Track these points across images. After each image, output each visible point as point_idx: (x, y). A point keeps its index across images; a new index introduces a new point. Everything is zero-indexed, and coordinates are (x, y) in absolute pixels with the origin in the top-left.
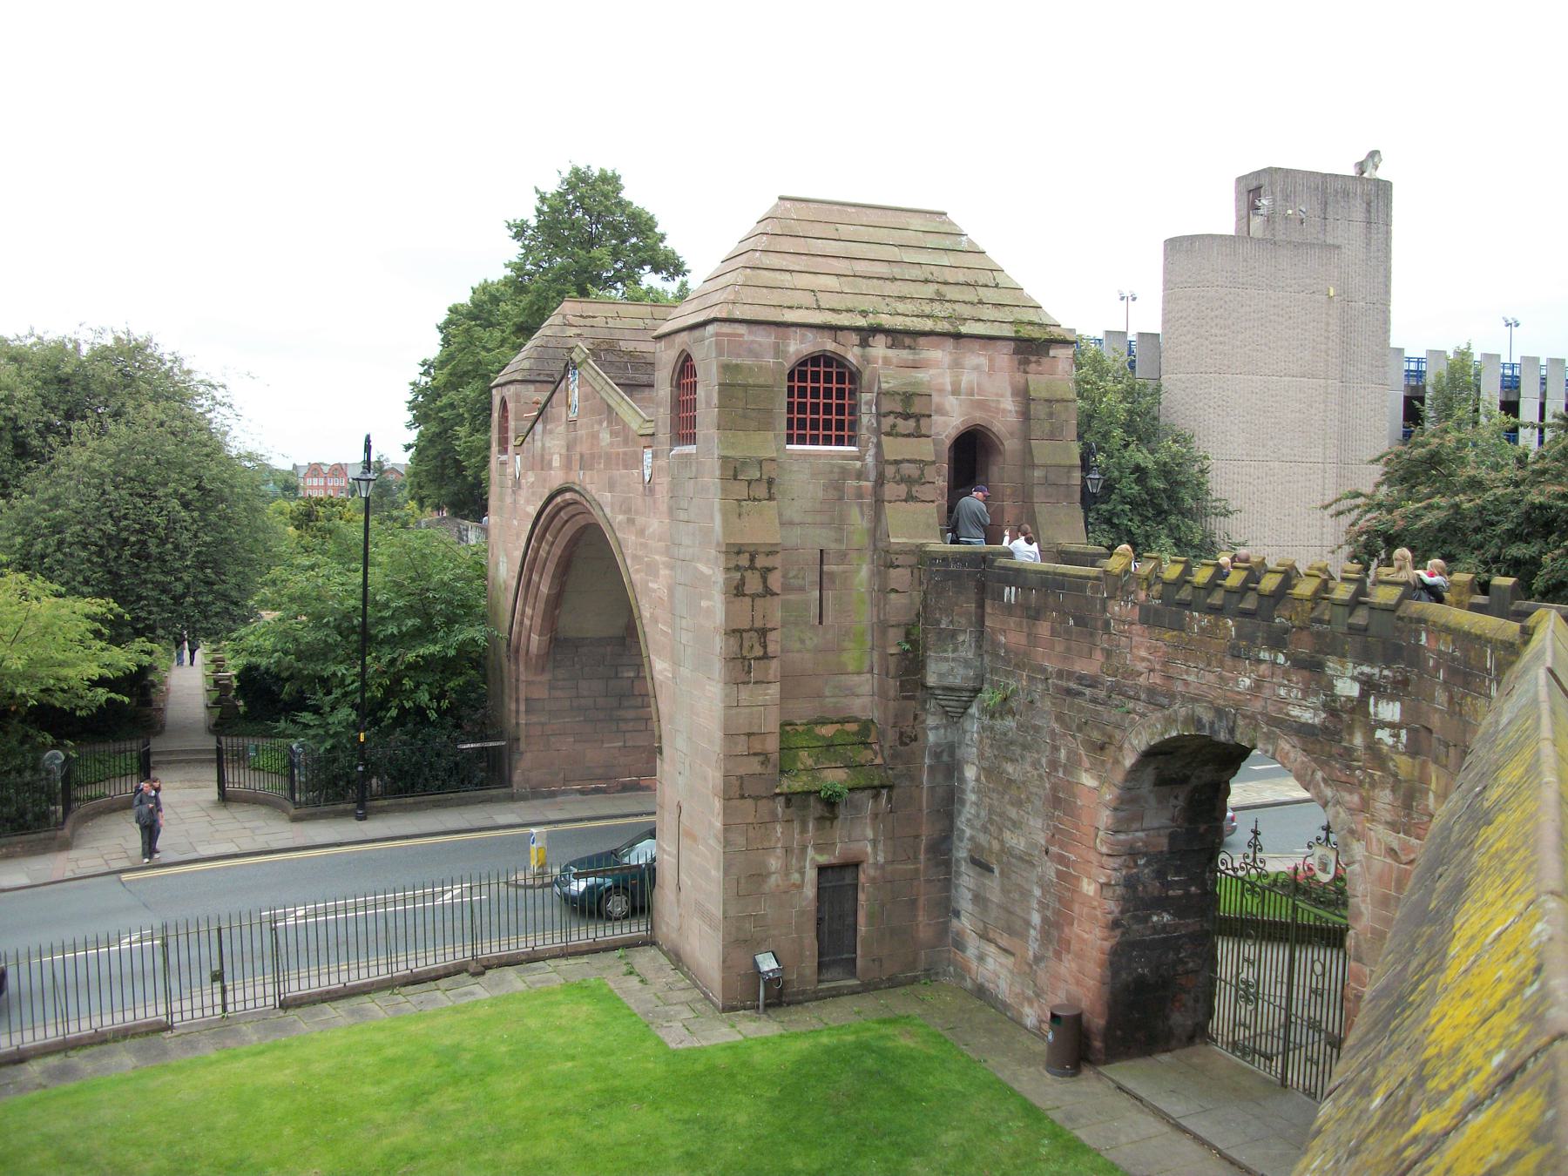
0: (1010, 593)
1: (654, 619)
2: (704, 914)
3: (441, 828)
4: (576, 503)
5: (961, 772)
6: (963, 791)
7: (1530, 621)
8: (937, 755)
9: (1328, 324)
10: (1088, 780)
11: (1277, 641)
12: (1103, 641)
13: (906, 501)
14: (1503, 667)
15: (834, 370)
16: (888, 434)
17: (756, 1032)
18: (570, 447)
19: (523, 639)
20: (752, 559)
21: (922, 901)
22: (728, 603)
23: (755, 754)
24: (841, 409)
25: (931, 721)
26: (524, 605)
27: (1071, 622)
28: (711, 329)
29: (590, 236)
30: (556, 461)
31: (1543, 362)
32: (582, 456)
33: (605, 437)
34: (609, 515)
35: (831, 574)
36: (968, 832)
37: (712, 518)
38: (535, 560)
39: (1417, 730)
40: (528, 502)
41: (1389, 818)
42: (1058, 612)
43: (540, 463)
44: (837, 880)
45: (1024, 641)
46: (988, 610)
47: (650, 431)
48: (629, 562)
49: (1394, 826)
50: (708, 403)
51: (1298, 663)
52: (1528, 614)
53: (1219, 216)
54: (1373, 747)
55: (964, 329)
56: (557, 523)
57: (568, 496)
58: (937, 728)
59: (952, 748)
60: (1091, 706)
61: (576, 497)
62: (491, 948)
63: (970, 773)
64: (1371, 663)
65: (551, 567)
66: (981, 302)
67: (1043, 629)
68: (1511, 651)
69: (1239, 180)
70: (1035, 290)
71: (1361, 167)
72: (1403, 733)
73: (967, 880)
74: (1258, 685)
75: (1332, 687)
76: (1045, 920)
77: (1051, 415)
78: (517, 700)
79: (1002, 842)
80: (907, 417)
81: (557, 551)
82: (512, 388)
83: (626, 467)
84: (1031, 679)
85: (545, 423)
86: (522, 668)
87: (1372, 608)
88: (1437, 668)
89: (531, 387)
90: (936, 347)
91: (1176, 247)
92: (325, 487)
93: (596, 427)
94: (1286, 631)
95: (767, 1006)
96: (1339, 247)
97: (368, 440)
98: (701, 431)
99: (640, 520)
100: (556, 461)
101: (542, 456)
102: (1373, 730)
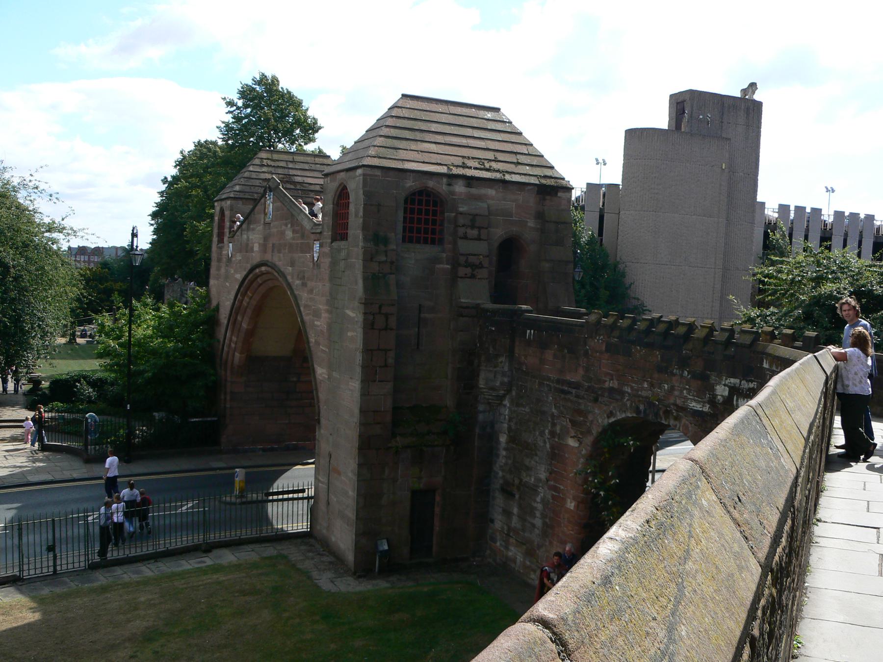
1: (317, 343)
3: (178, 469)
4: (268, 273)
5: (498, 439)
10: (572, 443)
11: (684, 363)
13: (470, 278)
15: (424, 198)
16: (461, 238)
17: (382, 584)
18: (266, 238)
20: (380, 308)
22: (365, 334)
25: (481, 408)
26: (232, 335)
27: (566, 351)
28: (359, 171)
29: (269, 112)
30: (256, 248)
31: (847, 214)
32: (273, 245)
33: (289, 234)
34: (290, 280)
36: (501, 474)
37: (356, 283)
38: (240, 307)
40: (236, 272)
43: (246, 248)
44: (421, 499)
47: (319, 231)
48: (302, 309)
50: (356, 216)
53: (659, 118)
55: (508, 177)
56: (255, 285)
57: (263, 269)
58: (484, 412)
60: (575, 399)
61: (269, 269)
62: (214, 536)
63: (503, 439)
65: (249, 312)
67: (549, 355)
69: (671, 96)
70: (550, 157)
71: (744, 91)
73: (499, 500)
74: (672, 389)
75: (714, 390)
79: (521, 480)
80: (473, 227)
82: (229, 202)
83: (302, 252)
85: (249, 224)
89: (240, 202)
90: (491, 188)
91: (631, 134)
92: (89, 262)
93: (284, 227)
96: (729, 139)
98: (351, 232)
99: (310, 284)
100: (256, 248)
101: (247, 245)
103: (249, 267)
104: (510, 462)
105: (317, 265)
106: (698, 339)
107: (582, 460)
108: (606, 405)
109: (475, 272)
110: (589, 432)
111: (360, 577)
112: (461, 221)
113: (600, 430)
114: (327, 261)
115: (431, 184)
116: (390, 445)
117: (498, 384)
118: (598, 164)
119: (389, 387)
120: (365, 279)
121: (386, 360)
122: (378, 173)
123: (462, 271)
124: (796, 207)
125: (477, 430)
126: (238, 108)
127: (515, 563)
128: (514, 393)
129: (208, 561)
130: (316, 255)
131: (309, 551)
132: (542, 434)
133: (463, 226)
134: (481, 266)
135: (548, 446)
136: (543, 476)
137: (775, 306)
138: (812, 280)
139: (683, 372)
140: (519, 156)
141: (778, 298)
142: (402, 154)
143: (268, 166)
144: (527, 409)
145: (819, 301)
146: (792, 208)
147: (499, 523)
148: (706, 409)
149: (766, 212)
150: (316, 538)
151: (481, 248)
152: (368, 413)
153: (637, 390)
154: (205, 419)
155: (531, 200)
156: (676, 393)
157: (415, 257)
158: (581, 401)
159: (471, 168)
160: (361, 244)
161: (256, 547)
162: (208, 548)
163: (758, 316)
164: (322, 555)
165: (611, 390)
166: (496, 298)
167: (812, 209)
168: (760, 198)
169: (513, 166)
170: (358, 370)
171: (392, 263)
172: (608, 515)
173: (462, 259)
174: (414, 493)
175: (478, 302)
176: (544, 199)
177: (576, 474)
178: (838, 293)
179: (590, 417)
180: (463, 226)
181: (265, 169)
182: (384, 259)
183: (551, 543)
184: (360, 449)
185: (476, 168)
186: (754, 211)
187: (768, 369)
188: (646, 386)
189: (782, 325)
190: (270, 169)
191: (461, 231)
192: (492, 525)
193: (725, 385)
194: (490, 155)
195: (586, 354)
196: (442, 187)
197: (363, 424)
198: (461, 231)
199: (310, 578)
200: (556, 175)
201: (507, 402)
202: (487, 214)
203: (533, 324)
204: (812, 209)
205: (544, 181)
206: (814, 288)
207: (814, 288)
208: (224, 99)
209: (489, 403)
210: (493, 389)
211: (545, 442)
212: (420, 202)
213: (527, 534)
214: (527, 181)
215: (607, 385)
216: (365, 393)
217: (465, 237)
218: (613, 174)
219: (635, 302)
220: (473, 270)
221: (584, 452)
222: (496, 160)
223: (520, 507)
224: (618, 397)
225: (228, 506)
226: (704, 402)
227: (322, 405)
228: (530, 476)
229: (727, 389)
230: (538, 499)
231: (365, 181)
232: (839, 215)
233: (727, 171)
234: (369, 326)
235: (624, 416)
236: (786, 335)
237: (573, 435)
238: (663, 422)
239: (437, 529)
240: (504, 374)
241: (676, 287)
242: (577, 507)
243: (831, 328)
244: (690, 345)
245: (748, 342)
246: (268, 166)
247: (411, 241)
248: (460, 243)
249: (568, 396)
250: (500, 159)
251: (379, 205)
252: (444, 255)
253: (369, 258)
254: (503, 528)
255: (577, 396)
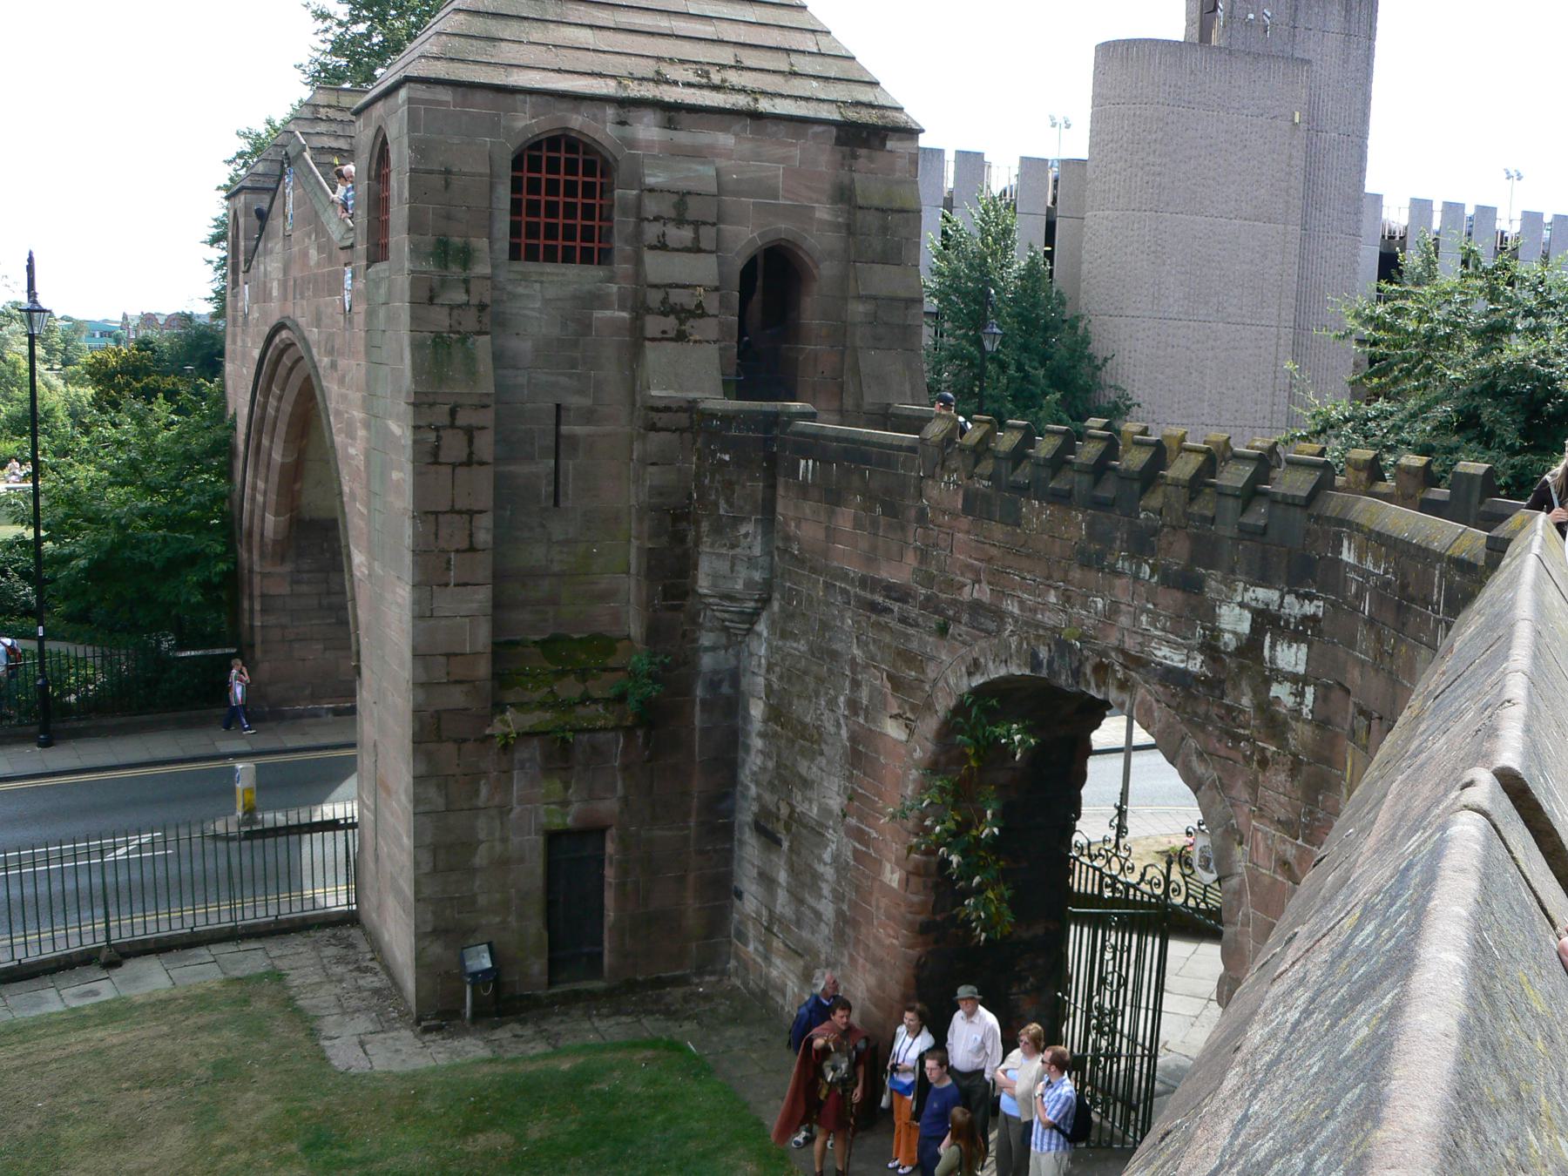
0: (805, 466)
2: (398, 892)
3: (145, 757)
6: (747, 734)
7: (1501, 531)
8: (713, 685)
9: (1290, 157)
10: (893, 730)
11: (1141, 545)
12: (915, 535)
14: (1459, 601)
15: (580, 158)
17: (469, 1051)
19: (256, 521)
20: (453, 413)
21: (691, 877)
22: (418, 474)
23: (456, 682)
24: (588, 212)
25: (706, 639)
26: (255, 476)
27: (879, 510)
28: (403, 93)
31: (1547, 219)
35: (573, 438)
36: (753, 790)
38: (263, 418)
39: (1327, 687)
41: (1282, 814)
42: (863, 495)
44: (570, 855)
45: (821, 535)
46: (781, 491)
47: (348, 243)
49: (1287, 826)
50: (400, 197)
51: (1169, 580)
52: (1502, 518)
54: (1266, 707)
55: (764, 105)
56: (282, 371)
57: (284, 334)
58: (713, 649)
59: (735, 677)
60: (900, 627)
63: (757, 710)
64: (1264, 581)
66: (795, 74)
67: (845, 519)
68: (1469, 579)
70: (871, 62)
72: (1310, 692)
73: (750, 850)
74: (1113, 610)
76: (840, 914)
77: (884, 229)
78: (251, 597)
79: (793, 811)
80: (680, 221)
81: (287, 407)
84: (828, 586)
86: (256, 557)
87: (1273, 499)
88: (1359, 596)
90: (726, 130)
94: (1156, 532)
95: (477, 1016)
96: (1309, 62)
97: (31, 259)
102: (1267, 682)
103: (267, 330)
104: (771, 765)
105: (348, 314)
106: (1176, 483)
107: (914, 774)
108: (964, 643)
109: (687, 327)
110: (929, 706)
111: (427, 1030)
112: (651, 207)
113: (952, 703)
114: (361, 308)
115: (577, 121)
116: (488, 731)
117: (739, 586)
118: (1054, 125)
119: (481, 597)
120: (416, 347)
121: (471, 535)
122: (445, 95)
123: (653, 325)
124: (1445, 203)
125: (699, 692)
126: (340, 24)
127: (784, 995)
128: (776, 606)
129: (106, 988)
130: (347, 298)
131: (340, 960)
132: (832, 704)
133: (656, 219)
134: (699, 312)
135: (844, 733)
136: (836, 803)
137: (1388, 398)
138: (1476, 334)
139: (1139, 567)
140: (794, 58)
141: (1396, 381)
142: (508, 53)
143: (329, 120)
144: (802, 646)
145: (1492, 385)
146: (1437, 207)
147: (751, 903)
148: (1196, 665)
149: (1384, 216)
150: (363, 927)
151: (703, 270)
152: (433, 660)
153: (1034, 611)
154: (210, 652)
155: (822, 156)
156: (1124, 621)
157: (543, 293)
158: (911, 631)
159: (675, 83)
160: (407, 265)
161: (224, 950)
162: (113, 957)
163: (1347, 420)
164: (367, 970)
165: (976, 607)
166: (740, 387)
167: (1478, 207)
168: (1370, 187)
169: (779, 79)
170: (408, 558)
171: (482, 307)
172: (976, 908)
173: (654, 298)
174: (553, 838)
175: (691, 395)
176: (854, 157)
177: (893, 817)
178: (1542, 363)
179: (931, 671)
180: (656, 219)
181: (322, 127)
182: (459, 297)
183: (852, 959)
184: (419, 740)
185: (689, 85)
186: (1358, 212)
187: (1354, 568)
188: (1053, 599)
189: (1403, 442)
190: (334, 127)
191: (652, 231)
192: (737, 902)
193: (1242, 605)
194: (725, 55)
195: (922, 517)
196: (603, 129)
197: (422, 685)
198: (652, 231)
199: (313, 1034)
200: (882, 101)
201: (762, 627)
202: (714, 190)
203: (812, 446)
204: (1478, 207)
205: (852, 115)
206: (1481, 353)
207: (1481, 353)
208: (307, 6)
209: (727, 629)
210: (730, 597)
211: (838, 725)
212: (553, 166)
213: (806, 934)
214: (811, 114)
215: (966, 595)
216: (423, 614)
217: (662, 246)
218: (1077, 146)
219: (1113, 396)
220: (682, 322)
221: (918, 754)
222: (739, 67)
223: (792, 870)
224: (992, 626)
225: (221, 845)
226: (1190, 649)
227: (361, 632)
228: (811, 801)
229: (1247, 615)
230: (827, 857)
231: (412, 115)
232: (1531, 220)
233: (1303, 126)
234: (428, 457)
235: (1003, 672)
236: (1409, 471)
237: (896, 711)
238: (1093, 692)
239: (610, 915)
240: (751, 562)
241: (1213, 368)
242: (906, 882)
243: (1522, 450)
244: (1155, 500)
245: (1304, 494)
246: (329, 120)
247: (532, 256)
248: (649, 257)
249: (884, 619)
250: (747, 63)
251: (448, 172)
252: (614, 288)
253: (426, 296)
254: (759, 914)
255: (903, 620)
